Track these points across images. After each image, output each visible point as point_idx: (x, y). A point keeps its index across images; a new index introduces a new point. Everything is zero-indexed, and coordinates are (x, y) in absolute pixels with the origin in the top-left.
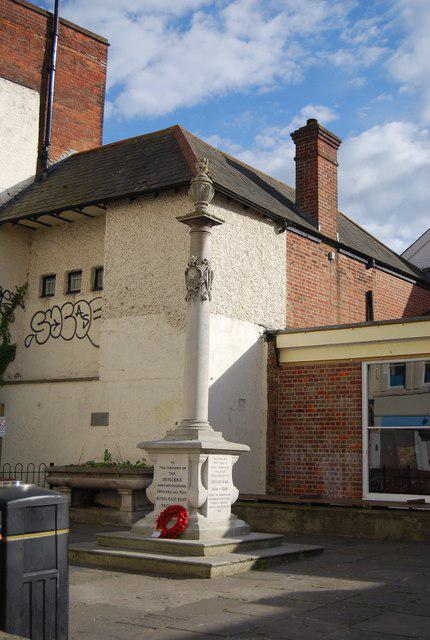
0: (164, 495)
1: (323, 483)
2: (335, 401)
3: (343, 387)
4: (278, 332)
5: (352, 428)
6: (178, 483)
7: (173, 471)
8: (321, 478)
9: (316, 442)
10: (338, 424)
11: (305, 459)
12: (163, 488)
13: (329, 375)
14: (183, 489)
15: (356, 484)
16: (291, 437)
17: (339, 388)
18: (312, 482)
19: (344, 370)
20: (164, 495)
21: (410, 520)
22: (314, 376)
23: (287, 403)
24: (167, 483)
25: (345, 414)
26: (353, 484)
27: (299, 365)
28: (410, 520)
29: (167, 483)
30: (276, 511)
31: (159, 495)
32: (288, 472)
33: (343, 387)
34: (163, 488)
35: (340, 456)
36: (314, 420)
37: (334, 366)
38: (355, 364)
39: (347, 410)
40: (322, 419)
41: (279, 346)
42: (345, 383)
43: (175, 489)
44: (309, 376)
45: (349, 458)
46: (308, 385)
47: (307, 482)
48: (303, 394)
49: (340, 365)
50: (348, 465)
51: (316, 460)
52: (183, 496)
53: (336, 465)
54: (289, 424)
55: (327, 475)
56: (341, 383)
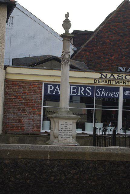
0: (62, 134)
1: (24, 126)
2: (31, 96)
3: (35, 91)
4: (8, 66)
5: (38, 106)
6: (68, 130)
7: (66, 125)
8: (23, 125)
9: (22, 111)
10: (32, 104)
11: (17, 118)
12: (62, 131)
13: (29, 86)
14: (70, 132)
15: (38, 127)
16: (10, 109)
17: (32, 91)
18: (20, 126)
19: (36, 84)
20: (62, 134)
21: (87, 139)
22: (22, 85)
23: (9, 95)
24: (63, 129)
25: (35, 101)
26: (37, 127)
27: (15, 80)
28: (87, 139)
29: (63, 129)
30: (37, 138)
31: (60, 134)
32: (8, 122)
33: (35, 91)
34: (62, 131)
35: (32, 117)
36: (21, 102)
37: (31, 82)
38: (40, 83)
39: (36, 99)
40: (26, 102)
41: (8, 72)
42: (36, 89)
43: (67, 132)
44: (20, 85)
45: (36, 117)
46: (19, 89)
47: (17, 126)
48: (17, 92)
49: (34, 82)
50: (35, 120)
51: (22, 118)
52: (70, 134)
53: (30, 120)
54: (9, 104)
55: (26, 124)
56: (34, 89)
